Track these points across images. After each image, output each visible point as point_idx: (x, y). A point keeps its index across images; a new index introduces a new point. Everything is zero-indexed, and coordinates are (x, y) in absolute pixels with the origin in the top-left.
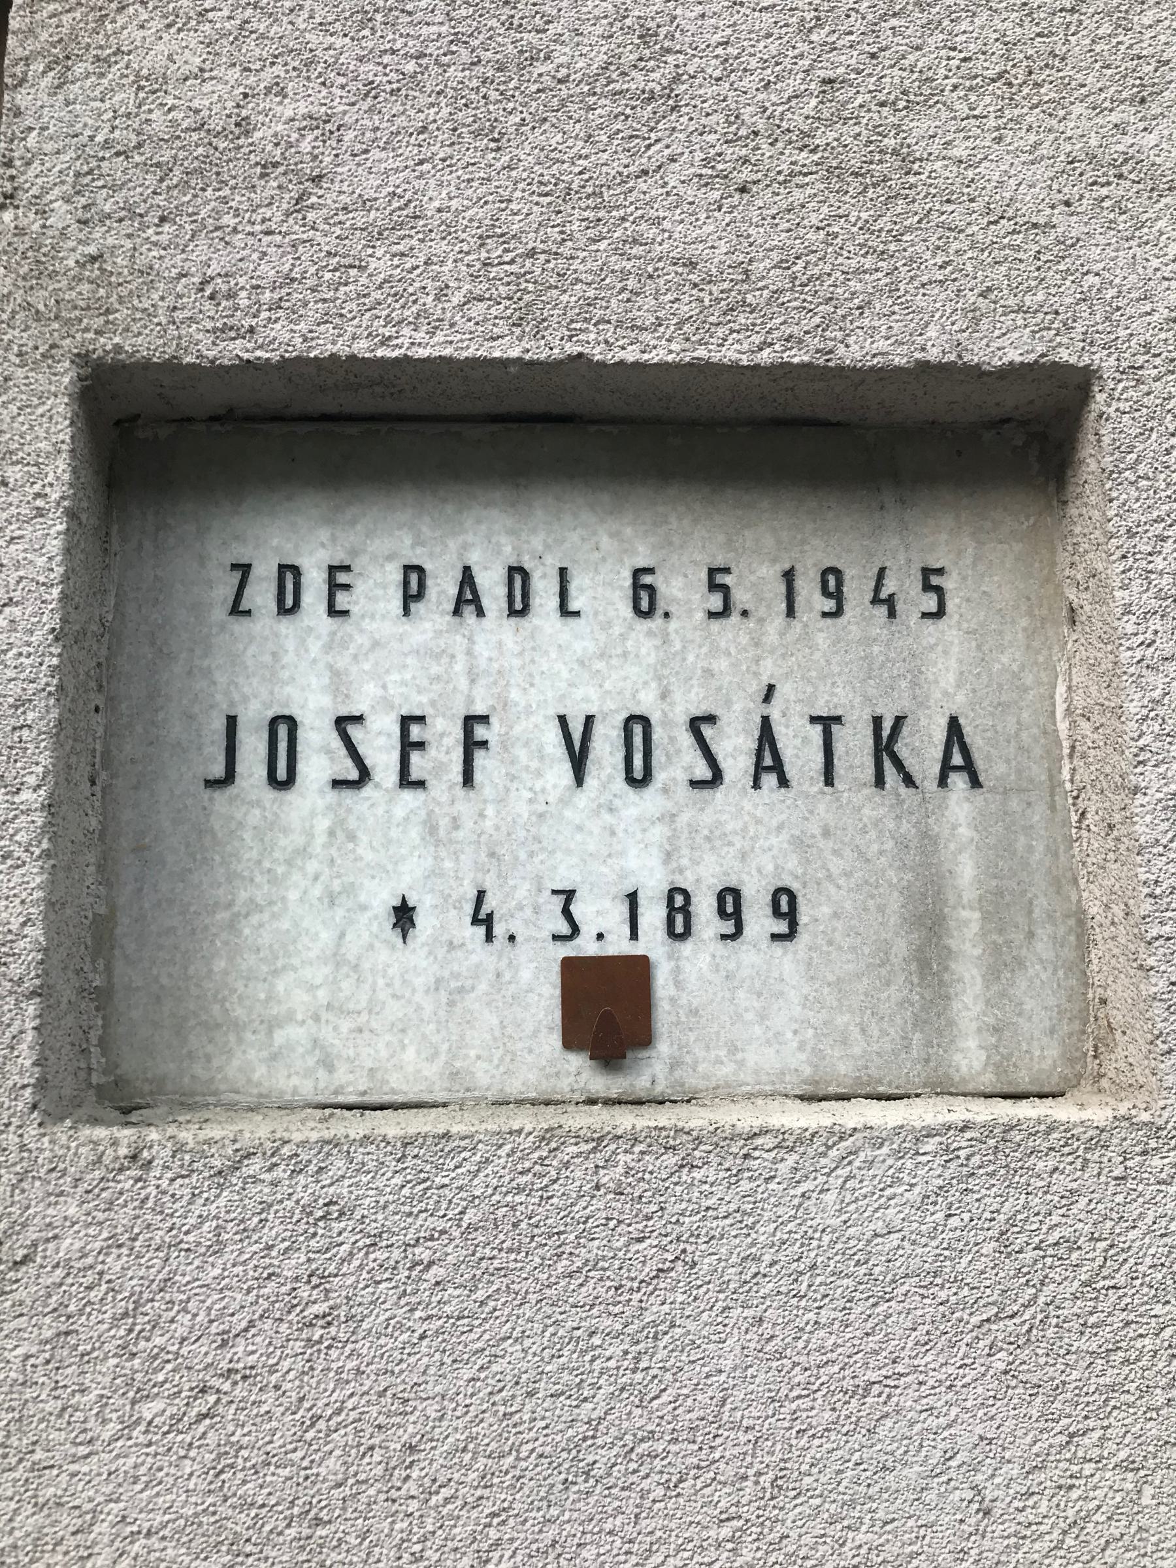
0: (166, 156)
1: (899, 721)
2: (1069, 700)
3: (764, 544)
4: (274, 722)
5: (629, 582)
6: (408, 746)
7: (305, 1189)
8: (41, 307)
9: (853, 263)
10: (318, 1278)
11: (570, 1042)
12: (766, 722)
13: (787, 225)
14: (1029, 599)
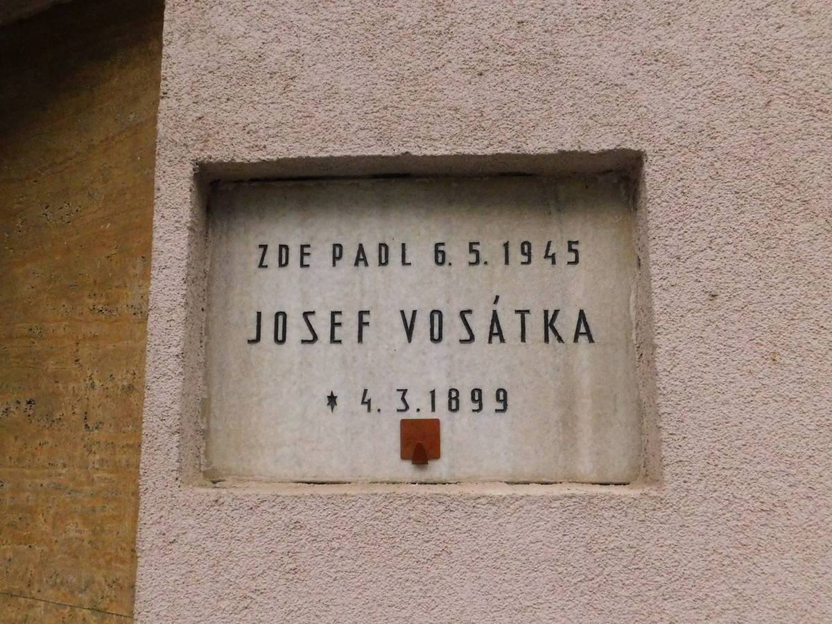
0: (230, 72)
1: (556, 312)
2: (636, 302)
3: (495, 230)
4: (277, 314)
5: (433, 249)
6: (334, 325)
7: (285, 516)
8: (178, 141)
9: (531, 107)
10: (291, 554)
11: (404, 457)
12: (495, 313)
13: (501, 90)
14: (618, 255)
